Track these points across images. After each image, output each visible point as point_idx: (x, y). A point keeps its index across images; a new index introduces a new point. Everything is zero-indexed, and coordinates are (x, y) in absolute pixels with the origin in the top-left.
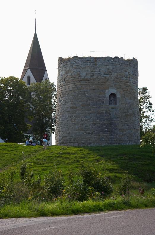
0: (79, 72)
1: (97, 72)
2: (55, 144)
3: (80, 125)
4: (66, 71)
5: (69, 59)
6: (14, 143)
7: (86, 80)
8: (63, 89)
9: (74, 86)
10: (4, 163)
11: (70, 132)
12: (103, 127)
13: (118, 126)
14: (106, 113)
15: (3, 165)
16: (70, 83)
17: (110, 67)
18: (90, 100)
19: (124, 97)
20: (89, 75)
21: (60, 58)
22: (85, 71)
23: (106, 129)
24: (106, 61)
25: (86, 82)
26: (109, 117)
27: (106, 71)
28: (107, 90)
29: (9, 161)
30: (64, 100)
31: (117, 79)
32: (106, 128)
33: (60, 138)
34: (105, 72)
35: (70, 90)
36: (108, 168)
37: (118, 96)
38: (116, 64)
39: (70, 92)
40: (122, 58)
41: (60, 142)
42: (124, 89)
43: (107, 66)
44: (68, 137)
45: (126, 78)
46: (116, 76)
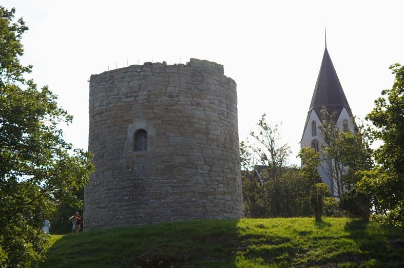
1: (115, 95)
12: (122, 193)
14: (128, 167)
17: (135, 83)
19: (165, 134)
22: (99, 97)
23: (126, 196)
24: (129, 73)
25: (101, 117)
26: (133, 174)
27: (129, 91)
28: (130, 126)
31: (148, 102)
32: (127, 195)
34: (127, 93)
36: (321, 236)
37: (151, 132)
38: (147, 76)
40: (164, 63)
42: (165, 119)
43: (129, 82)
45: (169, 99)
46: (147, 97)
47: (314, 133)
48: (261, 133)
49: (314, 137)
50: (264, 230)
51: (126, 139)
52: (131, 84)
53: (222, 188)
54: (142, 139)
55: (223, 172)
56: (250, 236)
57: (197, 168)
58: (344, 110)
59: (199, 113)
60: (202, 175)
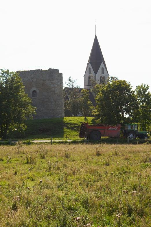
2: (64, 120)
6: (40, 138)
19: (42, 92)
28: (31, 89)
37: (38, 91)
40: (41, 69)
47: (90, 73)
48: (69, 83)
49: (90, 75)
50: (71, 121)
51: (30, 93)
52: (31, 76)
53: (59, 108)
54: (35, 93)
55: (59, 103)
56: (67, 123)
57: (51, 102)
58: (102, 63)
59: (52, 86)
60: (53, 104)
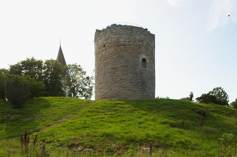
0: (119, 37)
3: (120, 83)
4: (106, 38)
5: (108, 27)
7: (124, 45)
8: (103, 54)
9: (114, 50)
10: (64, 112)
11: (111, 89)
13: (147, 85)
15: (64, 114)
16: (110, 48)
18: (128, 62)
20: (127, 41)
21: (97, 30)
22: (123, 37)
29: (68, 110)
30: (104, 63)
33: (102, 94)
34: (139, 40)
35: (111, 53)
37: (148, 61)
39: (111, 56)
41: (103, 97)
44: (110, 93)
